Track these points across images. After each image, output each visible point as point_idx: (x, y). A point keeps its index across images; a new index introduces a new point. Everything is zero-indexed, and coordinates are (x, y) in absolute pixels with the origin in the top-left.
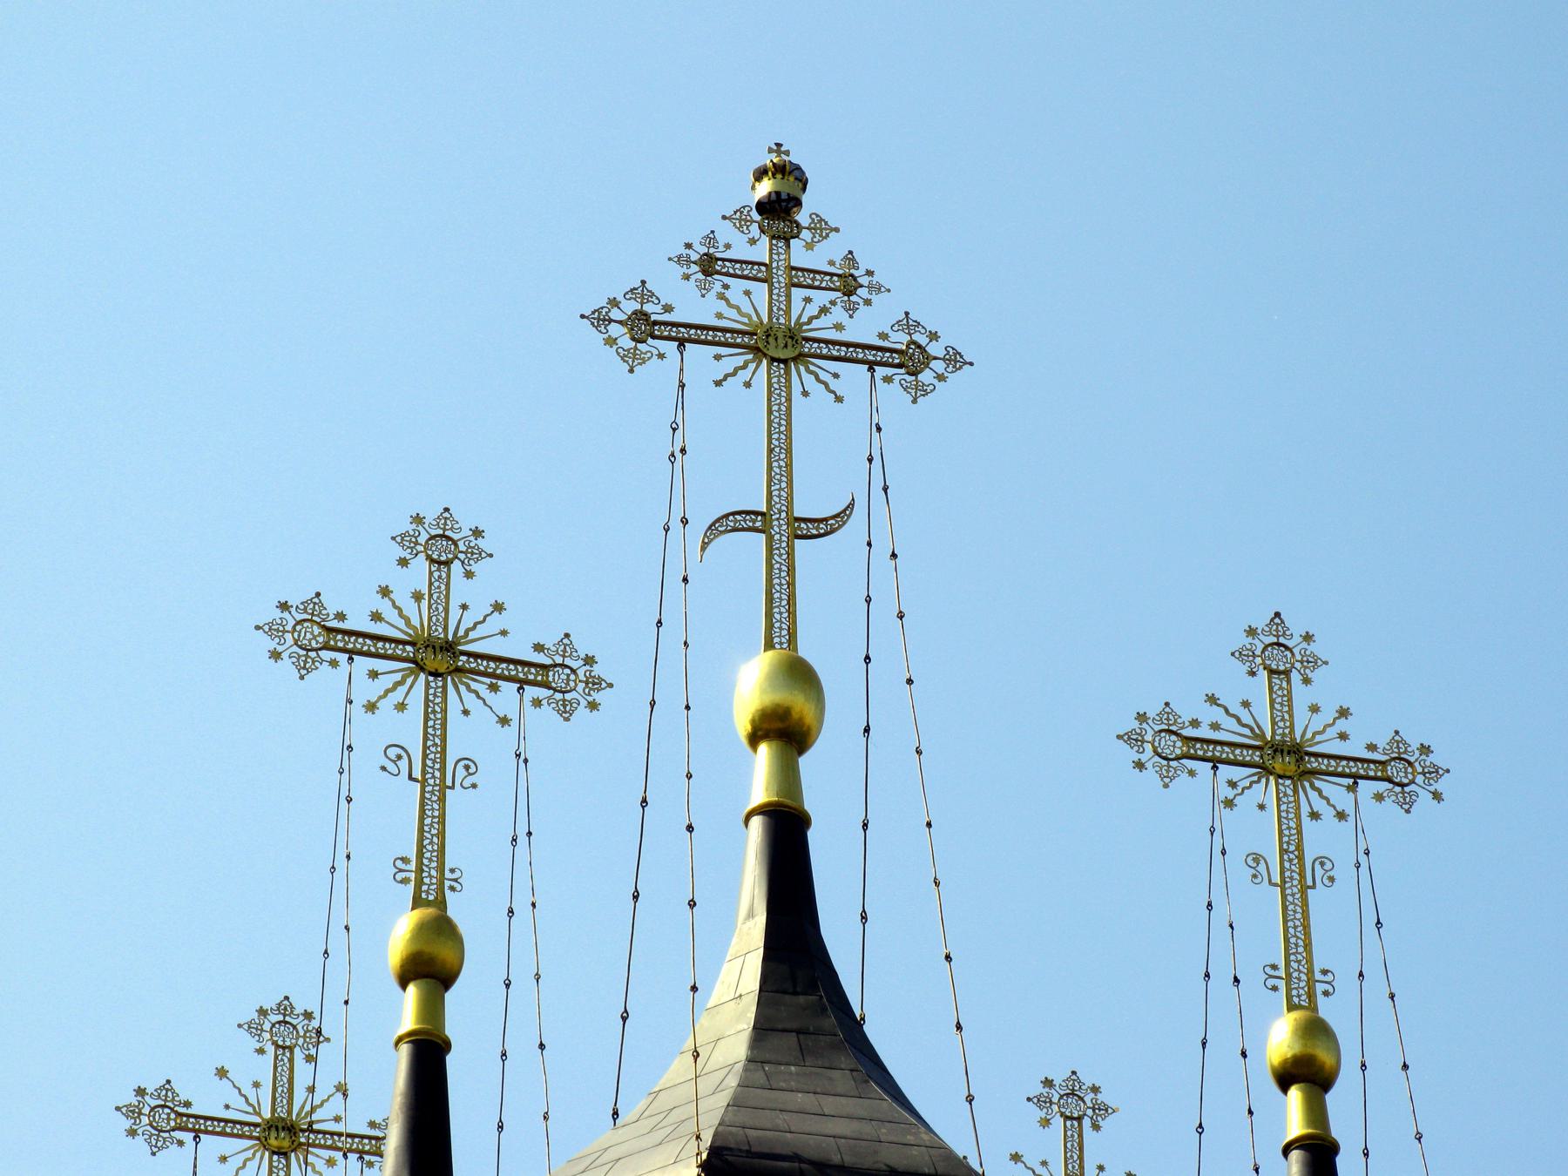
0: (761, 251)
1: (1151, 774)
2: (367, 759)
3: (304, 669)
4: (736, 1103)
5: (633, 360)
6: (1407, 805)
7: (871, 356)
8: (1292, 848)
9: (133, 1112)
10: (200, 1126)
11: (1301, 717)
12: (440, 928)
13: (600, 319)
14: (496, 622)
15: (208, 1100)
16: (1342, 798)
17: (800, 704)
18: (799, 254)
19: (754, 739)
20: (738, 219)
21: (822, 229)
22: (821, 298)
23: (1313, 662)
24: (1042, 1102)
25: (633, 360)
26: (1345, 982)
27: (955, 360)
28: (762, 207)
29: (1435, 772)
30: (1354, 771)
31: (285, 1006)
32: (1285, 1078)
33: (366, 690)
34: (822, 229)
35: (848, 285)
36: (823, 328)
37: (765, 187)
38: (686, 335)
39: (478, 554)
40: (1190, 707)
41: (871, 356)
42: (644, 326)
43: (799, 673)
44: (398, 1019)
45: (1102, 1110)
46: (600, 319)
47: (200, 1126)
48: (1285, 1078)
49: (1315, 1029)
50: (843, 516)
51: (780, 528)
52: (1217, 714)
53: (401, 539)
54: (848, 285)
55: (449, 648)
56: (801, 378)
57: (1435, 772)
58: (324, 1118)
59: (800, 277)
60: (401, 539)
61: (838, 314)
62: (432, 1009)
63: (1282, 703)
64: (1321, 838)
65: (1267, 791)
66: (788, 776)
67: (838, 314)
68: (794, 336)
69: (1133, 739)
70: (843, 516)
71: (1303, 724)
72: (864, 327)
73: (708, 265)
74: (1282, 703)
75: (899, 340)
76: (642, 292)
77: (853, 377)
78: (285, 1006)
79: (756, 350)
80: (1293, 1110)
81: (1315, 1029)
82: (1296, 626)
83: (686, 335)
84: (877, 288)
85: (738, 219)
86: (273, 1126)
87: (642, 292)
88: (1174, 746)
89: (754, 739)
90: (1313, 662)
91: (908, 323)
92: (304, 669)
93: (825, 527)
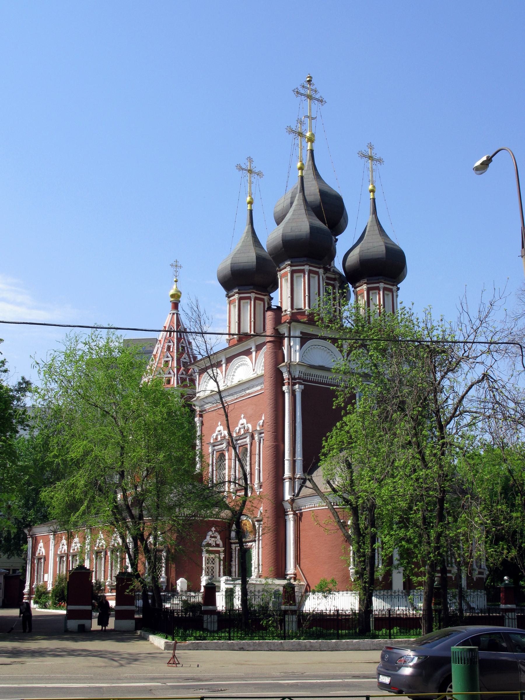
0: (308, 86)
1: (360, 158)
5: (297, 96)
6: (381, 164)
7: (318, 100)
10: (243, 169)
13: (294, 91)
15: (244, 167)
16: (376, 163)
25: (297, 96)
27: (325, 102)
28: (308, 81)
31: (250, 157)
36: (313, 96)
37: (308, 79)
38: (302, 94)
40: (363, 151)
41: (318, 100)
44: (298, 174)
47: (243, 169)
49: (374, 187)
52: (365, 152)
55: (302, 134)
61: (315, 94)
63: (371, 153)
67: (315, 94)
71: (373, 155)
73: (303, 86)
76: (297, 88)
78: (250, 157)
79: (308, 98)
80: (371, 195)
82: (372, 144)
83: (302, 94)
84: (318, 92)
86: (249, 170)
87: (297, 88)
88: (380, 161)
91: (321, 97)
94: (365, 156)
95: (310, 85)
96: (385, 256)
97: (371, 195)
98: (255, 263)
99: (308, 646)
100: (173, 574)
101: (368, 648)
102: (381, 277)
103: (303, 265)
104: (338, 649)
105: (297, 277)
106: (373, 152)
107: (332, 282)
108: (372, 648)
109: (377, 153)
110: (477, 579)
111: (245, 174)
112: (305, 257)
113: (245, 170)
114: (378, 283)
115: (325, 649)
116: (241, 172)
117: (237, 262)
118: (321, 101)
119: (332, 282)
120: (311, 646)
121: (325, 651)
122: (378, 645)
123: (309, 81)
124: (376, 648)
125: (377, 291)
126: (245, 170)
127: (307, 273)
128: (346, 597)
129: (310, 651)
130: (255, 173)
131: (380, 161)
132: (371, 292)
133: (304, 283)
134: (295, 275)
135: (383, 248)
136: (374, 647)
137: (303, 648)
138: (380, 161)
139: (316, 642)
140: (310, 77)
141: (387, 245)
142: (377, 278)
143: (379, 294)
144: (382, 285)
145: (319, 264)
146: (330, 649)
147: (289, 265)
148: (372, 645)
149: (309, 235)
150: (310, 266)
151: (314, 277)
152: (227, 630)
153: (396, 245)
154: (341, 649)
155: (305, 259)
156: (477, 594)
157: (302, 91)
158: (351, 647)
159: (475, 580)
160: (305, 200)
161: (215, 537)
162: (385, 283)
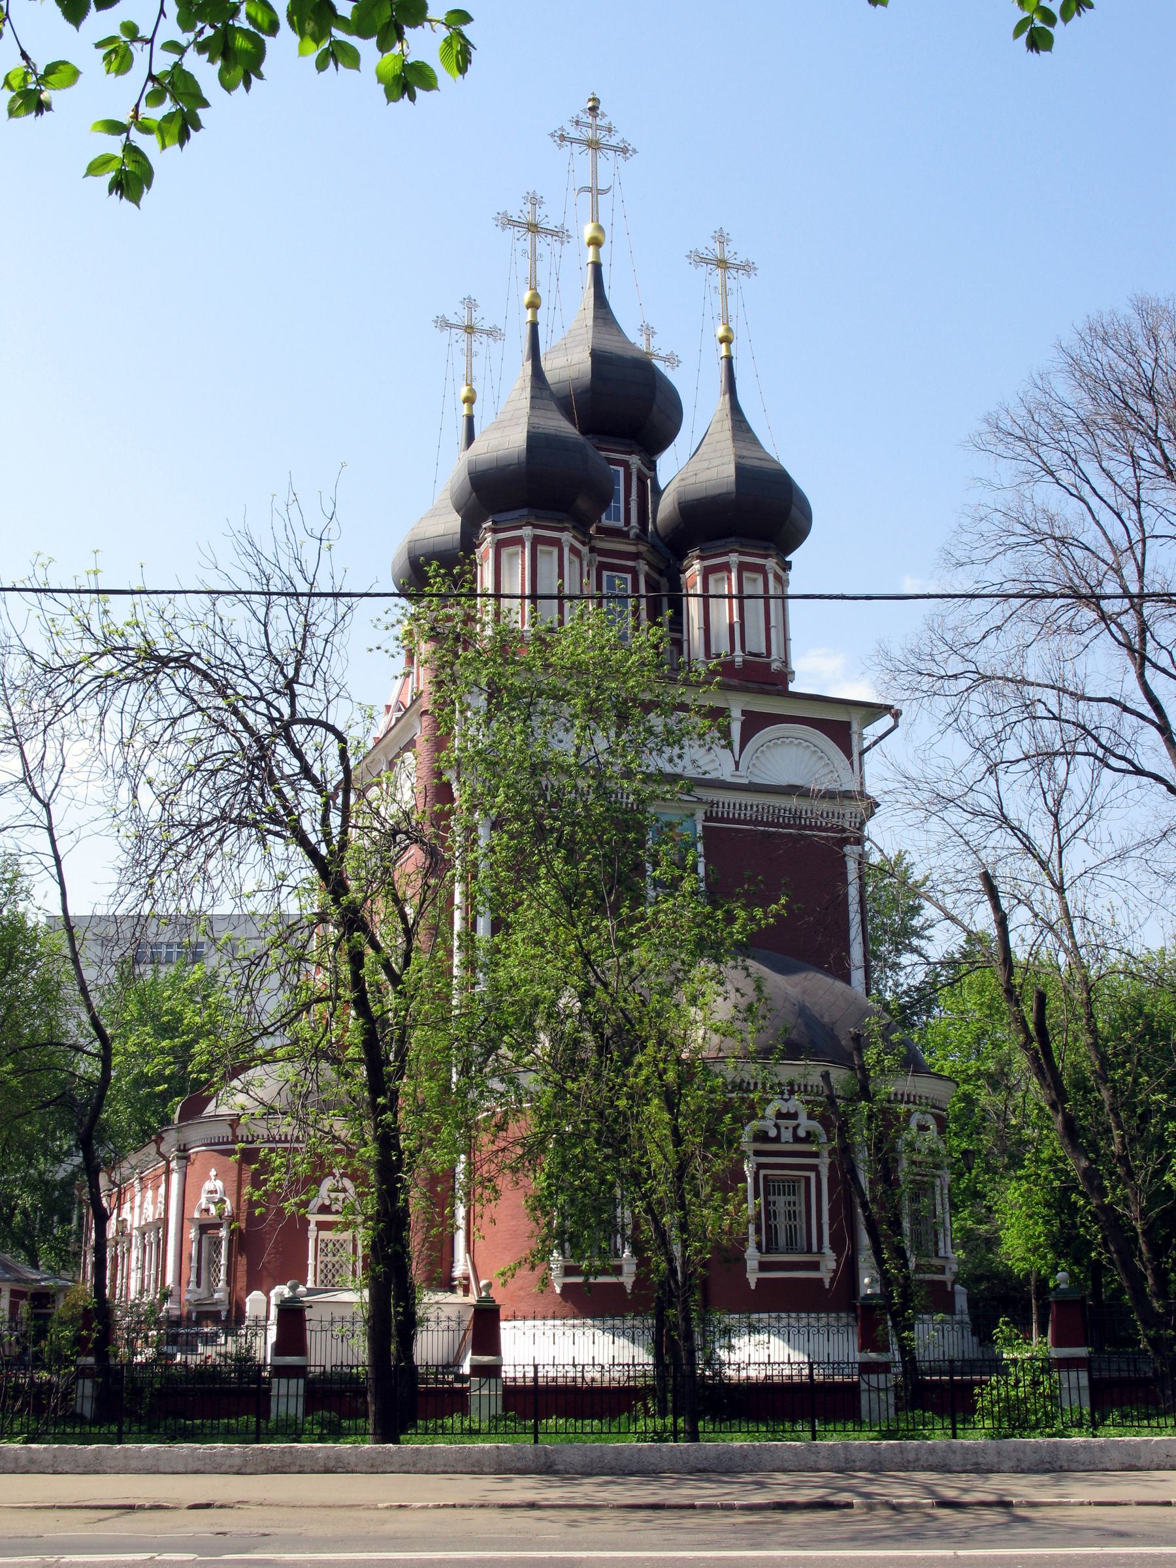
0: (590, 120)
2: (519, 253)
3: (503, 229)
4: (594, 337)
5: (560, 146)
6: (562, 243)
7: (615, 149)
8: (724, 286)
9: (436, 322)
10: (451, 326)
11: (726, 254)
12: (536, 296)
13: (552, 135)
14: (546, 220)
16: (735, 275)
17: (600, 236)
18: (599, 122)
19: (589, 244)
20: (584, 111)
21: (604, 115)
22: (604, 133)
23: (729, 240)
24: (641, 330)
25: (560, 146)
26: (734, 318)
27: (635, 151)
28: (590, 109)
29: (755, 269)
30: (738, 268)
31: (469, 298)
32: (722, 341)
33: (518, 235)
34: (604, 115)
35: (610, 130)
36: (604, 141)
37: (590, 104)
38: (573, 141)
39: (542, 203)
40: (702, 250)
41: (615, 149)
42: (563, 138)
43: (600, 228)
45: (654, 333)
46: (552, 135)
47: (451, 326)
48: (722, 341)
49: (729, 330)
50: (609, 189)
51: (594, 191)
52: (706, 252)
53: (524, 198)
54: (610, 130)
55: (536, 226)
56: (599, 154)
57: (755, 269)
58: (479, 326)
59: (599, 127)
60: (524, 198)
61: (607, 138)
62: (534, 315)
63: (723, 250)
64: (730, 284)
65: (719, 271)
66: (597, 254)
67: (607, 138)
68: (597, 142)
69: (689, 257)
70: (609, 189)
72: (613, 141)
73: (577, 123)
74: (723, 250)
75: (622, 145)
76: (562, 129)
77: (611, 154)
78: (469, 298)
79: (589, 146)
81: (729, 330)
82: (725, 231)
83: (573, 141)
85: (584, 111)
87: (562, 129)
88: (698, 259)
89: (589, 244)
90: (729, 240)
91: (623, 141)
92: (503, 229)
93: (605, 192)
94: (705, 261)
95: (595, 117)
96: (732, 487)
97: (723, 351)
98: (458, 536)
99: (24, 1461)
100: (242, 1282)
101: (181, 1468)
102: (733, 539)
103: (519, 527)
104: (100, 1468)
105: (717, 581)
106: (727, 249)
107: (630, 563)
108: (190, 1469)
109: (737, 251)
110: (760, 1281)
111: (457, 338)
112: (522, 507)
113: (457, 327)
114: (726, 554)
115: (66, 1468)
116: (446, 333)
117: (422, 537)
118: (625, 151)
119: (630, 563)
120: (32, 1461)
121: (67, 1473)
122: (207, 1461)
123: (593, 109)
124: (202, 1468)
125: (725, 574)
126: (457, 327)
127: (528, 545)
128: (435, 1333)
129: (27, 1472)
130: (482, 331)
131: (747, 268)
132: (712, 578)
133: (523, 569)
134: (505, 552)
135: (730, 471)
136: (199, 1465)
137: (11, 1466)
138: (747, 268)
139: (45, 1449)
140: (594, 99)
141: (742, 461)
142: (723, 541)
143: (729, 579)
144: (734, 558)
145: (560, 521)
146: (79, 1470)
147: (698, 557)
148: (190, 1460)
149: (524, 455)
150: (535, 526)
151: (755, 580)
152: (530, 1423)
153: (775, 461)
154: (109, 1470)
155: (525, 511)
156: (789, 1325)
157: (574, 133)
158: (134, 1464)
159: (753, 1287)
160: (538, 374)
161: (344, 1190)
162: (742, 553)
